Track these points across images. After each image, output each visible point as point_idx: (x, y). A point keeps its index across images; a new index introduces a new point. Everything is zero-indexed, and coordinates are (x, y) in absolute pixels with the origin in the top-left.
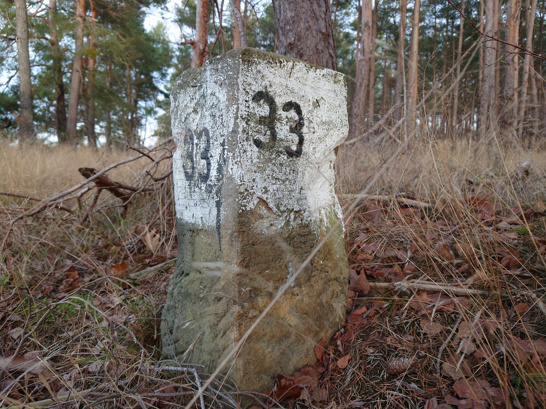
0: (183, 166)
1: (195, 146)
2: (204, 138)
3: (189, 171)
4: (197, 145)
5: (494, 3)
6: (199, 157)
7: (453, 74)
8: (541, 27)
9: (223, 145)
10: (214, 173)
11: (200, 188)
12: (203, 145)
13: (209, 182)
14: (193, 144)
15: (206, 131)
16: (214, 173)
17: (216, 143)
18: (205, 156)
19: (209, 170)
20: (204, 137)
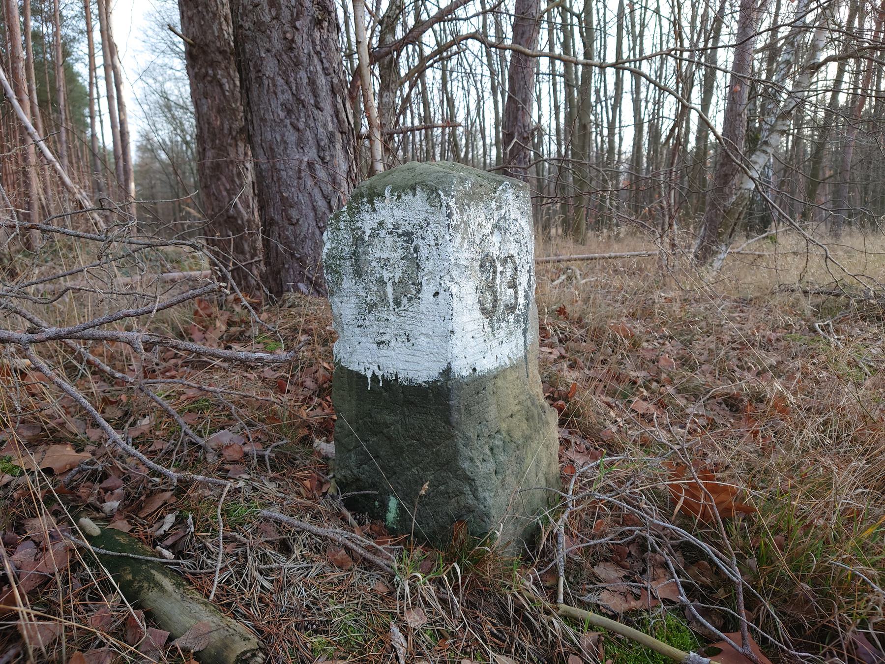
0: (479, 301)
1: (498, 274)
2: (509, 264)
3: (488, 306)
4: (501, 273)
5: (345, 7)
6: (505, 285)
7: (274, 577)
8: (847, 34)
9: (529, 272)
10: (521, 300)
11: (508, 322)
12: (509, 273)
13: (517, 312)
14: (495, 272)
15: (511, 257)
16: (521, 300)
17: (523, 270)
18: (513, 285)
19: (516, 298)
20: (509, 264)
